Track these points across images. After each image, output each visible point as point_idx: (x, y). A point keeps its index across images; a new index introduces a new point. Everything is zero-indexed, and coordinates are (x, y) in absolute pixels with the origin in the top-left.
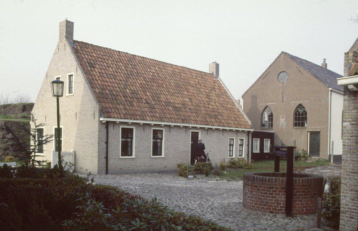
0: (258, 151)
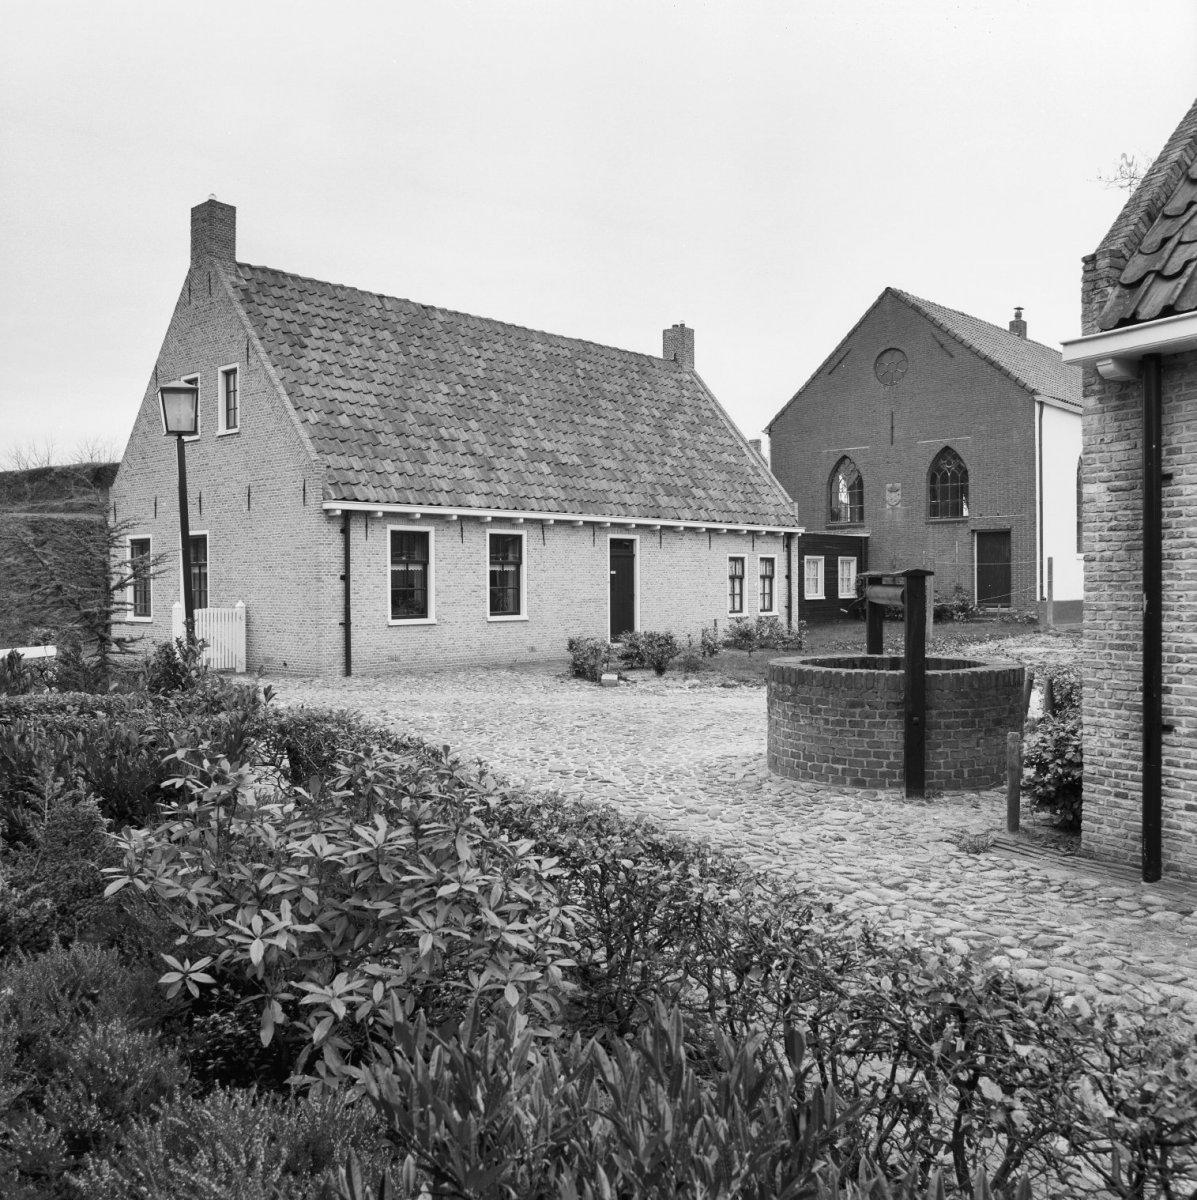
0: (820, 596)
